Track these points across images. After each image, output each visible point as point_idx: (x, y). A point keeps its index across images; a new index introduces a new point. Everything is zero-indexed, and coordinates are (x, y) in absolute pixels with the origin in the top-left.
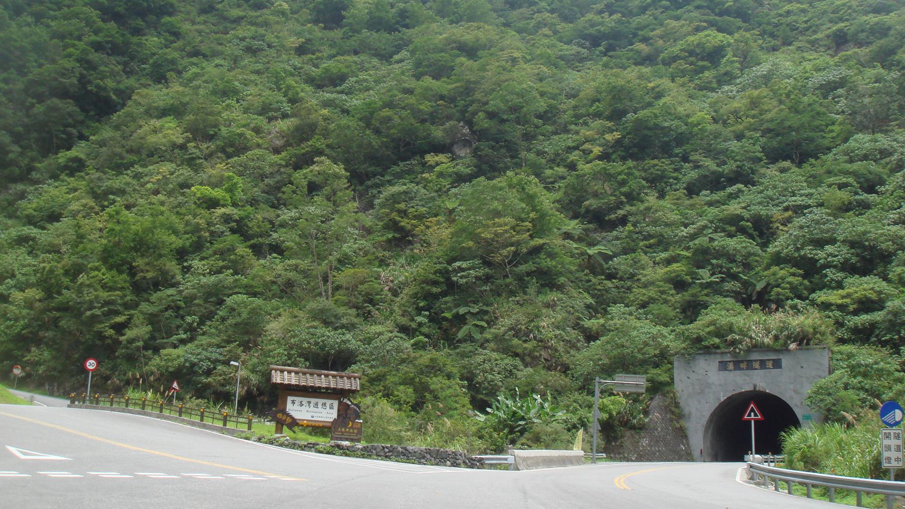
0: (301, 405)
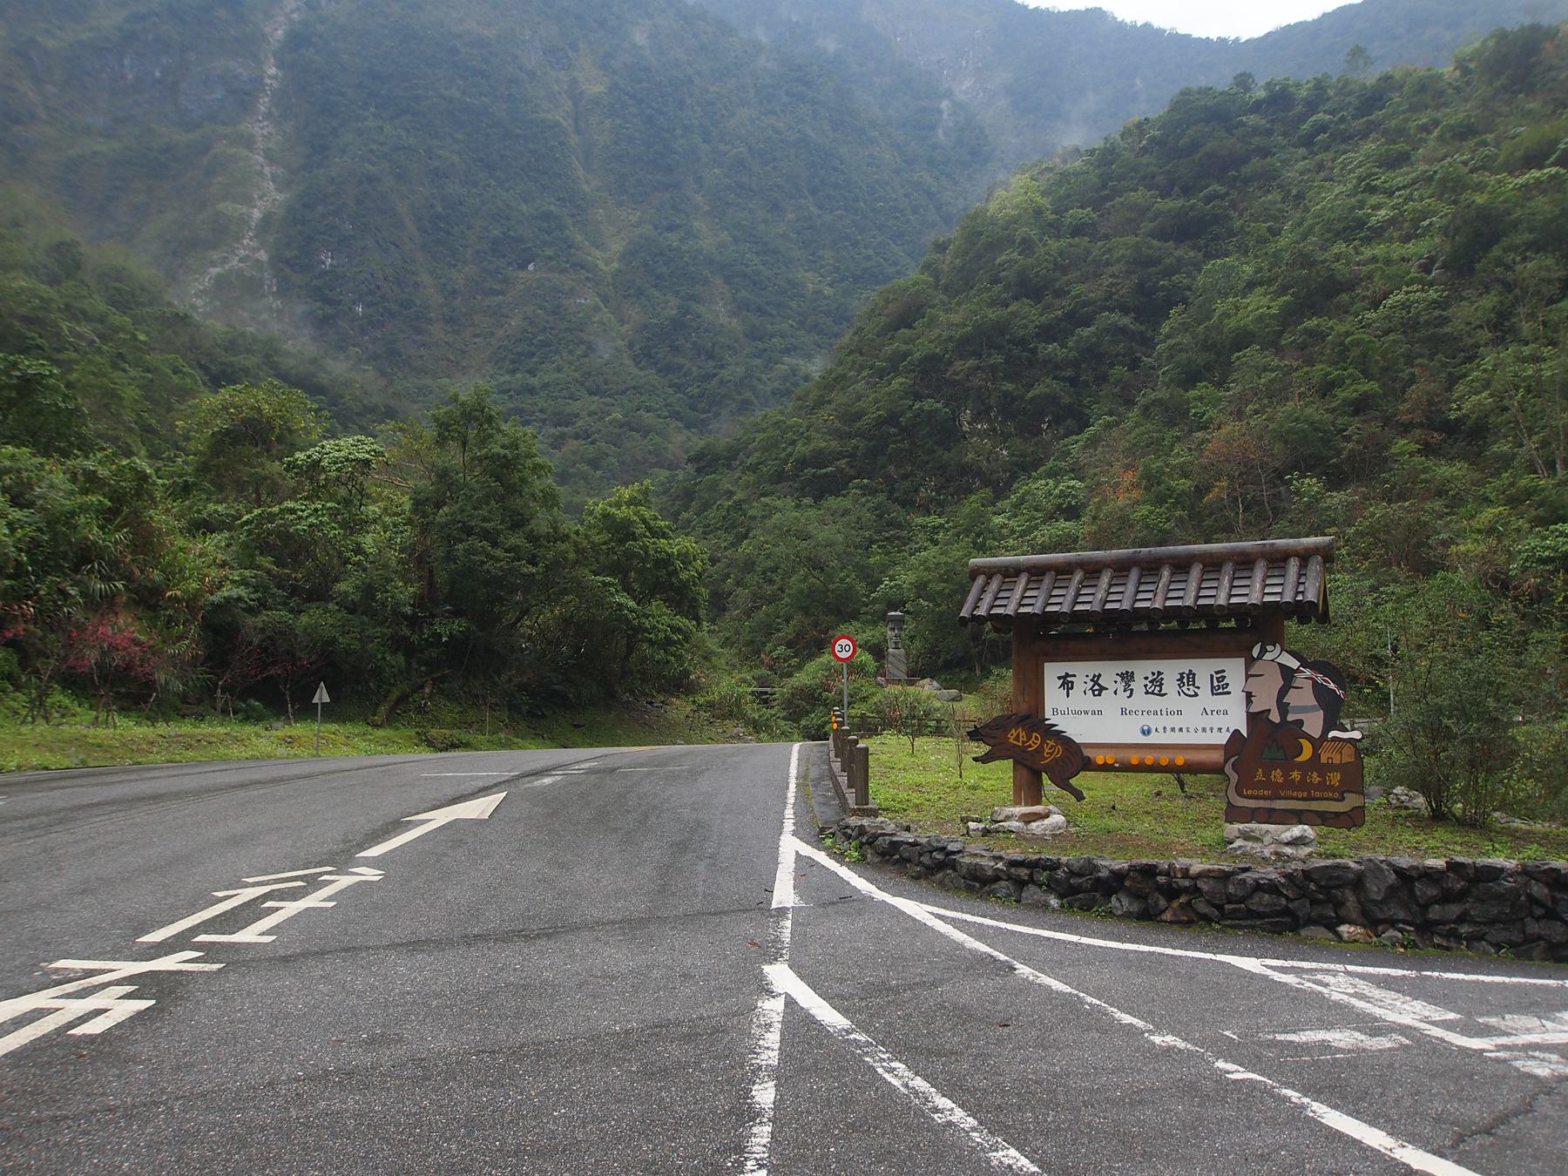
0: (1098, 689)
